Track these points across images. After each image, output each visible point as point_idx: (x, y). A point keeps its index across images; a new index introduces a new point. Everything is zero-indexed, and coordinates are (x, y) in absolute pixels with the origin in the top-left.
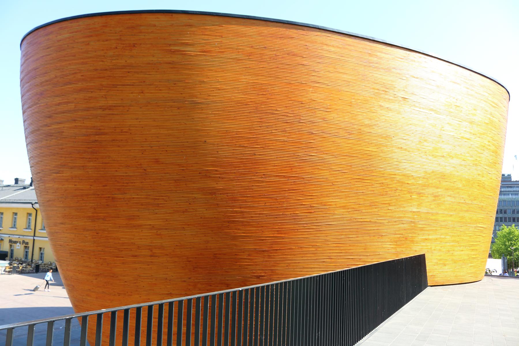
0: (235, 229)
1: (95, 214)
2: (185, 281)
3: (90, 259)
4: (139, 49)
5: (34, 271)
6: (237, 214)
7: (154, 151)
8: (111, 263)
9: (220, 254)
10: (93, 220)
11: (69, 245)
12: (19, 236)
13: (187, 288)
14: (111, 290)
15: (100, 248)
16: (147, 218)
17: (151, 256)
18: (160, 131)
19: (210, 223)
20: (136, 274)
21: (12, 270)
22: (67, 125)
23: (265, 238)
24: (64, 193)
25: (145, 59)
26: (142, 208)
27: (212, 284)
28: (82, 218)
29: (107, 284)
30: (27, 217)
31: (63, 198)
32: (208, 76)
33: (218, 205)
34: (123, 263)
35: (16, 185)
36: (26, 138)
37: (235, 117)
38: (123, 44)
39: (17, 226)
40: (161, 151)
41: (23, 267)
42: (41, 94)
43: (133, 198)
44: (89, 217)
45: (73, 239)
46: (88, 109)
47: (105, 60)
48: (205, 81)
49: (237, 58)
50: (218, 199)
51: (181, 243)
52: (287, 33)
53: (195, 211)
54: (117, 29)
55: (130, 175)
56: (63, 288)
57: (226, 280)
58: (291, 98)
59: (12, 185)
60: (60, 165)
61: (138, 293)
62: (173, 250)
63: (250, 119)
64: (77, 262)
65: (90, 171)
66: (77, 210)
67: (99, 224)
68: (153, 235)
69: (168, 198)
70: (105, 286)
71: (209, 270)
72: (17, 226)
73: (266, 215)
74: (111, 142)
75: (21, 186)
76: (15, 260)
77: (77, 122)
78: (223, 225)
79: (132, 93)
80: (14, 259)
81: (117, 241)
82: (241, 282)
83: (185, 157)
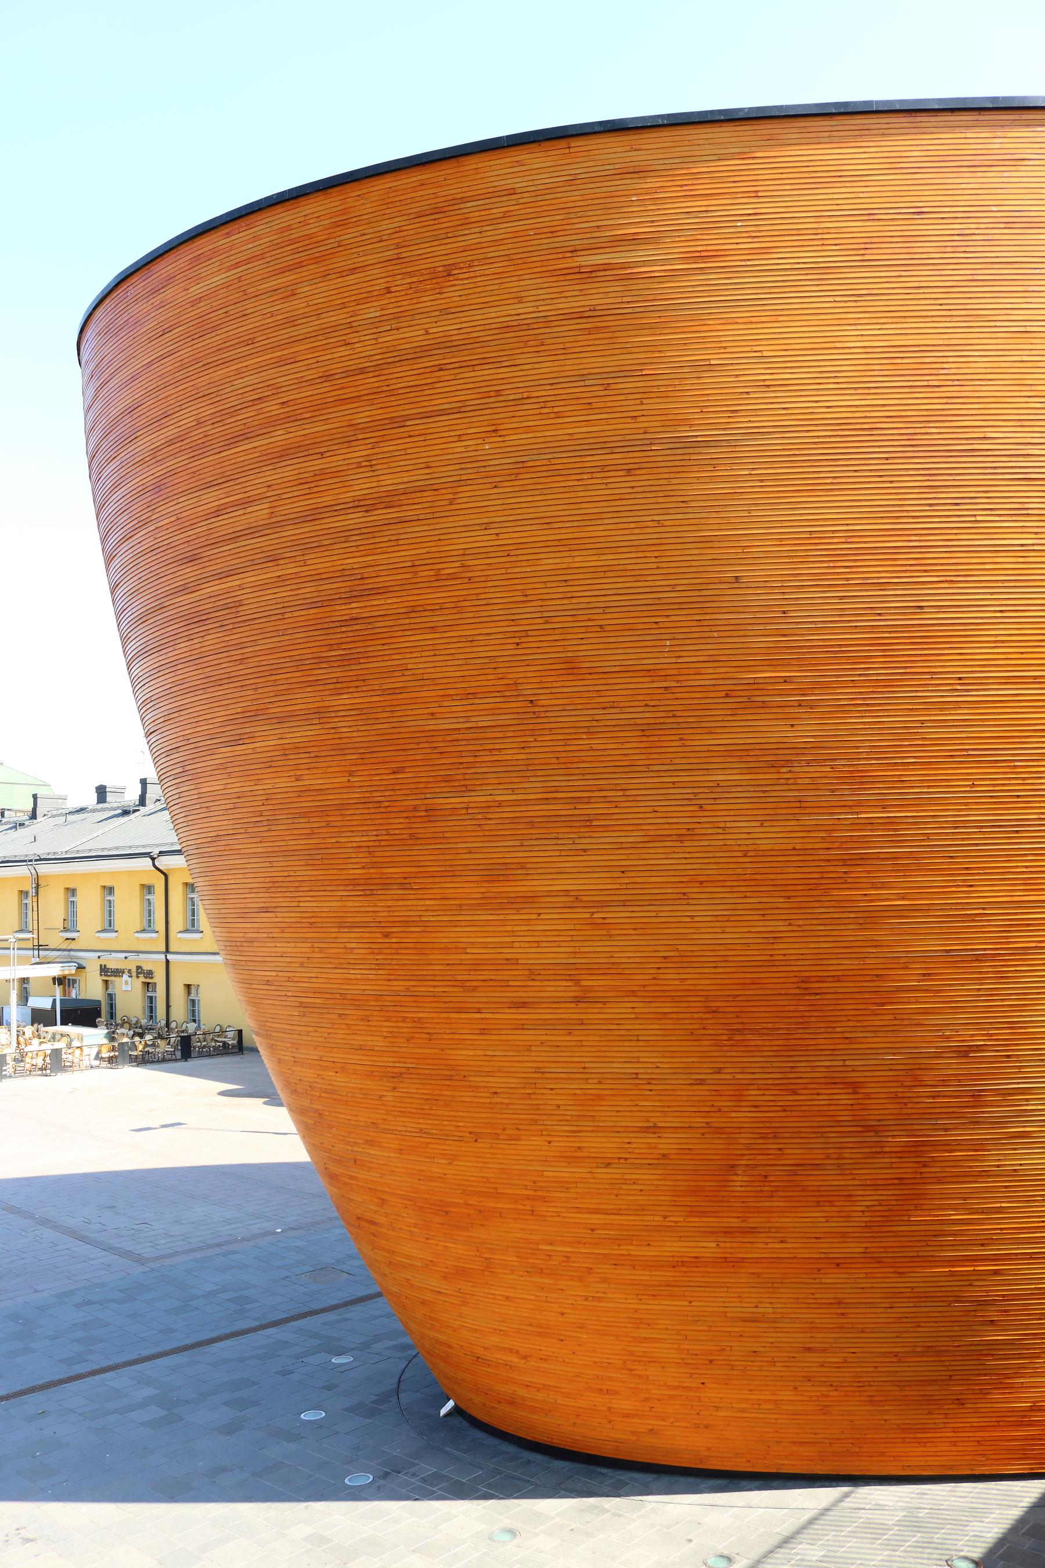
0: (869, 886)
1: (372, 871)
2: (701, 1079)
3: (370, 1023)
4: (465, 282)
5: (178, 1054)
6: (872, 830)
7: (557, 631)
8: (442, 1031)
9: (822, 980)
10: (368, 892)
11: (295, 979)
12: (127, 955)
13: (710, 1104)
14: (446, 1123)
15: (399, 986)
16: (555, 870)
17: (577, 1000)
18: (570, 560)
19: (779, 870)
20: (529, 1064)
21: (117, 1053)
22: (250, 578)
23: (982, 912)
24: (263, 808)
25: (494, 315)
26: (533, 837)
27: (797, 1087)
28: (329, 888)
29: (435, 1102)
30: (142, 896)
31: (260, 824)
32: (723, 345)
33: (804, 805)
34: (483, 1032)
35: (101, 805)
36: (124, 641)
37: (834, 481)
38: (410, 274)
39: (117, 925)
40: (583, 630)
41: (146, 1045)
42: (158, 488)
43: (500, 804)
44: (354, 882)
45: (305, 960)
46: (313, 515)
47: (355, 340)
48: (712, 362)
49: (821, 265)
50: (800, 781)
51: (681, 948)
52: (996, 144)
53: (721, 831)
54: (384, 227)
55: (480, 724)
56: (265, 1103)
57: (850, 1069)
58: (1034, 388)
59: (90, 807)
60: (240, 716)
61: (542, 1130)
62: (655, 976)
63: (891, 482)
64: (326, 1035)
65: (344, 724)
66: (310, 862)
67: (389, 903)
68: (578, 927)
69: (621, 793)
70: (428, 1112)
71: (785, 1037)
72: (116, 925)
73: (980, 825)
74: (405, 616)
75: (115, 809)
76: (122, 1026)
77: (282, 562)
78: (825, 875)
79: (460, 438)
80: (119, 1021)
81: (453, 958)
82: (904, 1073)
83: (668, 643)
